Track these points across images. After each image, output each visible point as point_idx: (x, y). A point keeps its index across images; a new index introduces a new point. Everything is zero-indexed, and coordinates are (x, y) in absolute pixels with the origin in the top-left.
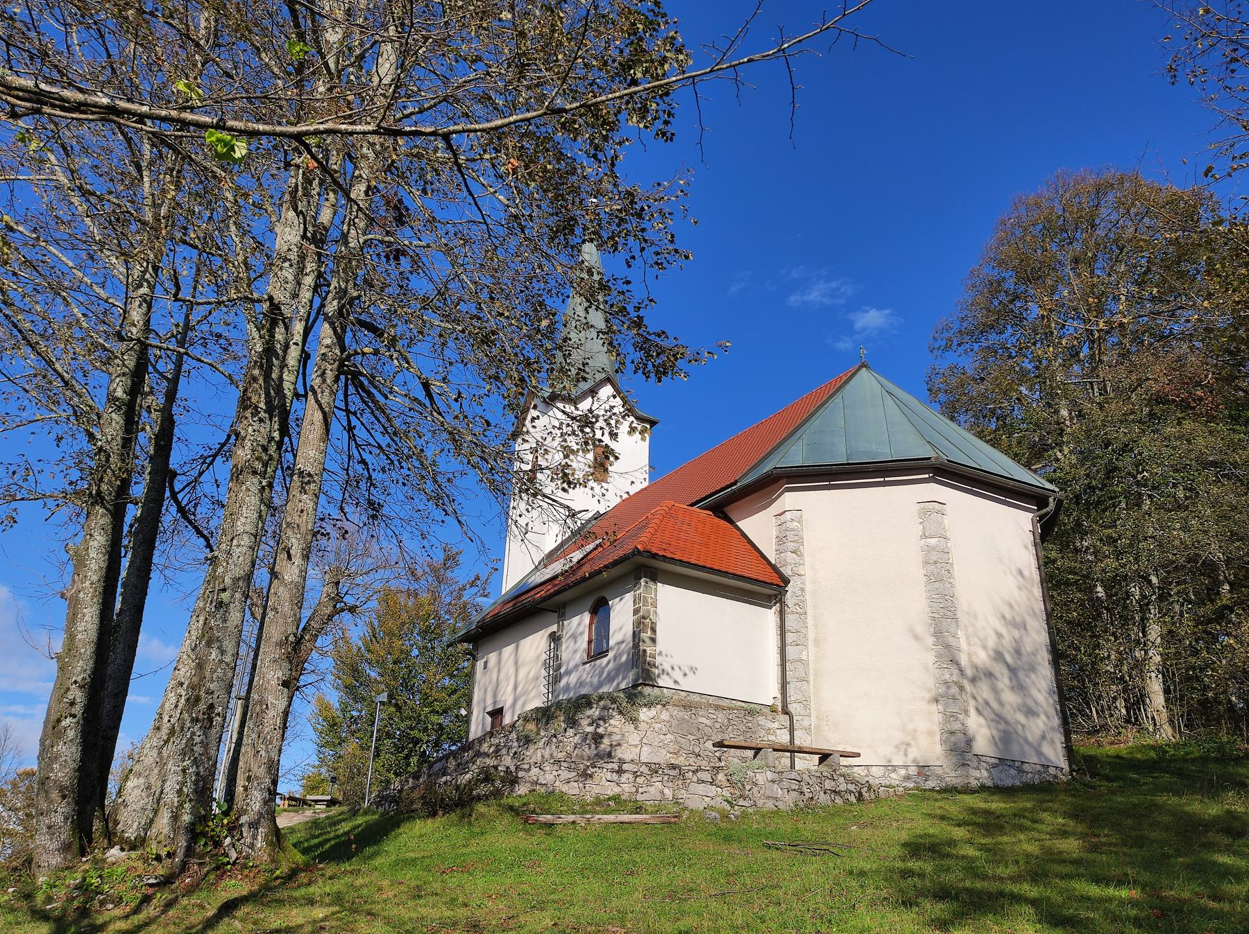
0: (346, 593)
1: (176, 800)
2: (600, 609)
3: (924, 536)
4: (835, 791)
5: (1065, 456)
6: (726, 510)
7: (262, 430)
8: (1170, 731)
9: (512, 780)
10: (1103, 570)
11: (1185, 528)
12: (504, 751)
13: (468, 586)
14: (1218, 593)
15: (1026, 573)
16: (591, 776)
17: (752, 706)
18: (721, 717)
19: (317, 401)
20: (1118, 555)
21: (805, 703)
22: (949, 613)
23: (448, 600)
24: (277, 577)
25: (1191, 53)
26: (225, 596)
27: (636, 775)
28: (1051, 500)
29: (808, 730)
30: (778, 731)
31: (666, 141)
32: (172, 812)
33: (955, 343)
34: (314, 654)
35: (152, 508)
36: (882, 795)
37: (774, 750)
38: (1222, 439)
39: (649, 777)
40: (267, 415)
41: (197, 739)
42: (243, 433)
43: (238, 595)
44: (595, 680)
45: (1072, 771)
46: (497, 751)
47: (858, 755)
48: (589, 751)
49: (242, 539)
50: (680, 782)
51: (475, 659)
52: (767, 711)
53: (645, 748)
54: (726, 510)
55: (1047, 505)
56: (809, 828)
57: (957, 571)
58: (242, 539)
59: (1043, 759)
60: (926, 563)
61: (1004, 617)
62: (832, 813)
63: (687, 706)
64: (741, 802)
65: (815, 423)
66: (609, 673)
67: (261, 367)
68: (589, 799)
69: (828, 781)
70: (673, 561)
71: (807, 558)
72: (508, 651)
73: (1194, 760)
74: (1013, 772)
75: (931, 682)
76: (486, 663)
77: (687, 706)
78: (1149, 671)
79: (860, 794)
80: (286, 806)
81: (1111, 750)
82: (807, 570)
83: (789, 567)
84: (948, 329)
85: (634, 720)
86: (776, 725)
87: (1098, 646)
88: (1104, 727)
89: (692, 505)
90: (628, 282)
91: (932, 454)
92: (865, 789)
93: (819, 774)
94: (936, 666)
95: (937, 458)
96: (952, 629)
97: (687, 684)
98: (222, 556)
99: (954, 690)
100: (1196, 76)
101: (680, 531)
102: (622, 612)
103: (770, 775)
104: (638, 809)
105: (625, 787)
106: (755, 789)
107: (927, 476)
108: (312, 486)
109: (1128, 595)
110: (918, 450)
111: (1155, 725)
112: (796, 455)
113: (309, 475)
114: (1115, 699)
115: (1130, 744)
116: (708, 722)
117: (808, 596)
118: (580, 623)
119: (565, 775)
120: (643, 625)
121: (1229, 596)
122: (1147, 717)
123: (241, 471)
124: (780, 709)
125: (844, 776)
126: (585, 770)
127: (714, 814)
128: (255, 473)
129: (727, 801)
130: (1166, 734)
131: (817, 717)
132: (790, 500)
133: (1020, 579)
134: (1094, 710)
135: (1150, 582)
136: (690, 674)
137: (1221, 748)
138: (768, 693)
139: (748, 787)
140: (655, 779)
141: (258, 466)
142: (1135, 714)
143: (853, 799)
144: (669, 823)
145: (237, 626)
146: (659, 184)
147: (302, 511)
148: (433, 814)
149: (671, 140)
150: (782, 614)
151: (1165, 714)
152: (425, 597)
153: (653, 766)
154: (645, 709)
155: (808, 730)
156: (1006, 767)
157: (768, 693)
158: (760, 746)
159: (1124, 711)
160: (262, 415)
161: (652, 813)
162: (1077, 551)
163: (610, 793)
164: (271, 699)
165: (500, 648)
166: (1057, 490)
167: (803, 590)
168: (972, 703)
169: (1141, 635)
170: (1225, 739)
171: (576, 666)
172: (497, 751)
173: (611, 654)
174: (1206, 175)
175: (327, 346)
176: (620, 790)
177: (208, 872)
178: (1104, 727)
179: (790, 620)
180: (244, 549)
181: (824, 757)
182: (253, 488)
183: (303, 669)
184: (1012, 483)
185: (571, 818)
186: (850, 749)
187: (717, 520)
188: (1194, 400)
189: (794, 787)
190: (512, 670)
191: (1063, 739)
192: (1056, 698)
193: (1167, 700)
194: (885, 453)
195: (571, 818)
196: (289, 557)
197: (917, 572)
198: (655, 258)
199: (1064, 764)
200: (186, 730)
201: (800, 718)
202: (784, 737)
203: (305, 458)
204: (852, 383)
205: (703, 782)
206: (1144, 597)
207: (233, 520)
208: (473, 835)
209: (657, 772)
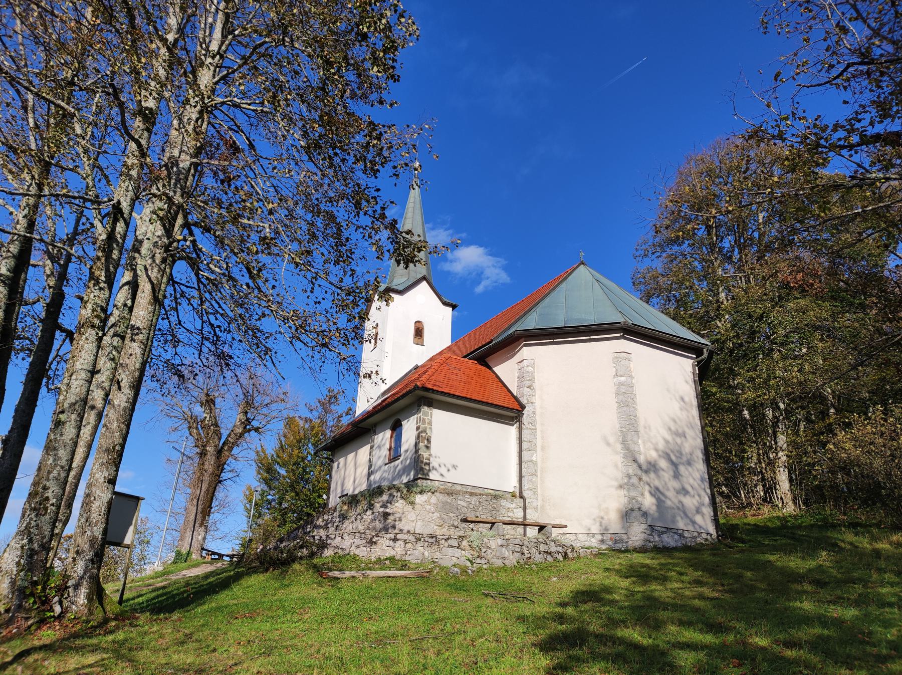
0: (253, 419)
1: (15, 569)
2: (396, 427)
3: (616, 376)
4: (547, 552)
5: (722, 324)
6: (487, 360)
7: (102, 296)
8: (793, 507)
9: (323, 545)
10: (746, 400)
11: (800, 371)
12: (330, 525)
13: (344, 415)
14: (828, 415)
15: (686, 399)
16: (375, 543)
17: (497, 492)
18: (474, 500)
19: (148, 276)
20: (756, 389)
21: (534, 491)
22: (633, 428)
23: (331, 424)
24: (109, 403)
25: (778, 11)
26: (63, 417)
27: (406, 542)
28: (705, 350)
29: (536, 508)
30: (515, 510)
31: (395, 82)
32: (11, 578)
33: (650, 252)
34: (230, 459)
35: (41, 355)
36: (582, 555)
37: (504, 523)
38: (826, 311)
39: (414, 544)
40: (106, 285)
41: (33, 524)
42: (86, 298)
43: (74, 416)
44: (390, 476)
45: (718, 536)
46: (327, 524)
47: (566, 526)
48: (378, 525)
49: (80, 375)
50: (436, 547)
51: (332, 461)
52: (509, 496)
53: (419, 523)
54: (487, 360)
55: (702, 354)
56: (520, 580)
57: (639, 399)
58: (80, 375)
59: (697, 527)
60: (617, 394)
61: (670, 429)
62: (543, 568)
63: (450, 493)
64: (478, 561)
65: (547, 301)
66: (399, 471)
67: (103, 251)
68: (373, 559)
69: (542, 545)
70: (443, 393)
71: (538, 392)
72: (351, 456)
73: (806, 527)
74: (676, 537)
75: (619, 475)
76: (339, 464)
77: (450, 493)
78: (779, 467)
79: (566, 554)
80: (210, 560)
81: (751, 520)
82: (537, 400)
83: (525, 398)
84: (645, 242)
85: (412, 503)
86: (514, 505)
87: (744, 451)
88: (750, 505)
89: (465, 357)
90: (378, 190)
91: (622, 320)
92: (570, 550)
93: (536, 541)
94: (623, 464)
95: (625, 323)
96: (635, 439)
97: (451, 477)
98: (63, 388)
99: (634, 480)
100: (782, 28)
101: (452, 373)
102: (409, 428)
103: (500, 542)
104: (404, 566)
105: (398, 550)
106: (489, 551)
107: (618, 335)
108: (141, 336)
109: (764, 416)
110: (613, 317)
111: (783, 503)
112: (531, 322)
113: (138, 328)
114: (756, 486)
115: (766, 516)
116: (465, 504)
117: (538, 418)
118: (384, 437)
119: (358, 542)
120: (423, 438)
121: (834, 417)
122: (778, 498)
123: (83, 325)
124: (518, 495)
125: (554, 541)
126: (371, 539)
127: (456, 569)
128: (93, 326)
129: (468, 560)
130: (790, 508)
131: (543, 500)
132: (528, 352)
133: (682, 403)
134: (742, 493)
135: (779, 408)
136: (452, 470)
137: (825, 519)
138: (511, 484)
139: (484, 550)
140: (419, 545)
141: (97, 322)
142: (770, 496)
143: (560, 557)
144: (423, 577)
145: (72, 439)
146: (408, 126)
147: (131, 355)
148: (267, 570)
149: (398, 81)
150: (520, 429)
151: (790, 496)
152: (316, 421)
153: (418, 536)
154: (419, 496)
155: (536, 508)
156: (672, 534)
157: (511, 484)
158: (493, 521)
159: (762, 494)
160: (102, 285)
161: (412, 569)
162: (730, 386)
163: (388, 555)
164: (98, 492)
165: (346, 455)
166: (709, 344)
167: (534, 413)
168: (647, 487)
169: (773, 442)
170: (829, 512)
171: (380, 467)
172: (327, 524)
173: (402, 458)
174: (776, 79)
175: (158, 237)
176: (395, 552)
177: (32, 625)
178: (750, 505)
179: (525, 433)
180: (81, 382)
181: (542, 528)
182: (91, 339)
183: (223, 469)
184: (677, 339)
185: (353, 573)
186: (557, 522)
187: (480, 367)
188: (807, 286)
189: (517, 549)
190: (353, 470)
191: (712, 514)
192: (707, 485)
193: (791, 485)
194: (591, 319)
195: (353, 573)
196: (120, 388)
197: (611, 401)
198: (394, 171)
199: (712, 529)
200: (26, 516)
201: (530, 500)
202: (519, 514)
203: (137, 317)
204: (573, 275)
205: (452, 547)
206: (775, 417)
207: (74, 361)
208: (283, 586)
209: (420, 540)
